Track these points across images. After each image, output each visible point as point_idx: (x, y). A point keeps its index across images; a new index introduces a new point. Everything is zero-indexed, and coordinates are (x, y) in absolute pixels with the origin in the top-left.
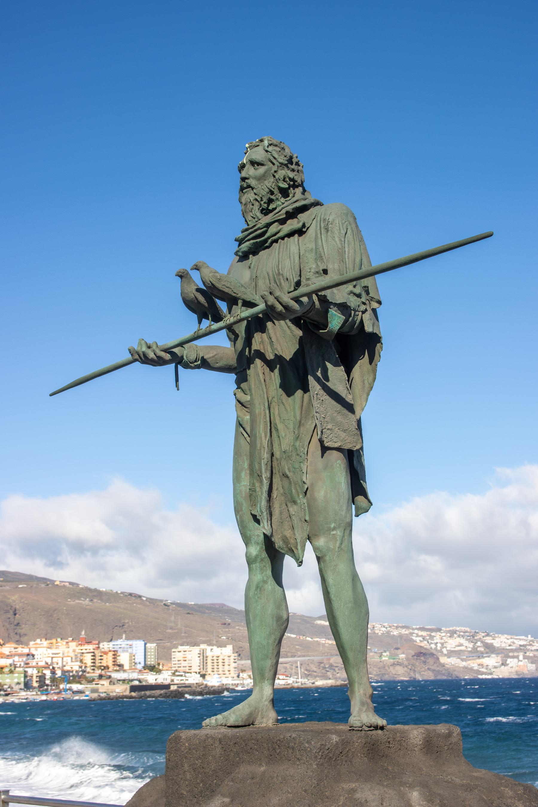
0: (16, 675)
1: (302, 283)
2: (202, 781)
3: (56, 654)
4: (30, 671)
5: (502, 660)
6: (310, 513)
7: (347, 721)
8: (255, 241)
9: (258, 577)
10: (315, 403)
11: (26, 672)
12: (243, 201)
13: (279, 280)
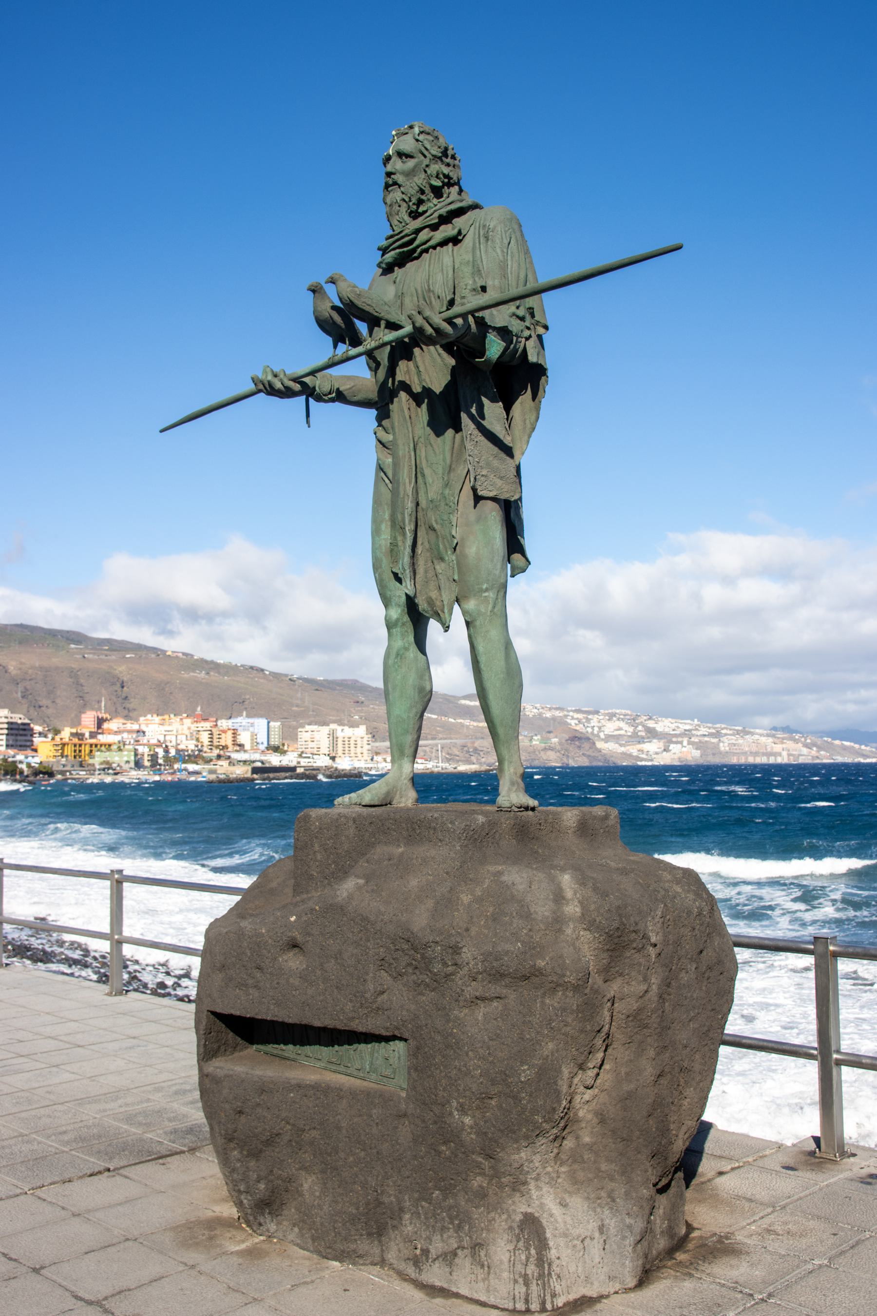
0: (126, 753)
1: (456, 302)
2: (334, 862)
3: (168, 731)
4: (141, 749)
5: (664, 746)
6: (459, 573)
7: (493, 802)
8: (401, 250)
9: (399, 643)
10: (469, 445)
11: (136, 750)
12: (388, 201)
13: (430, 298)
